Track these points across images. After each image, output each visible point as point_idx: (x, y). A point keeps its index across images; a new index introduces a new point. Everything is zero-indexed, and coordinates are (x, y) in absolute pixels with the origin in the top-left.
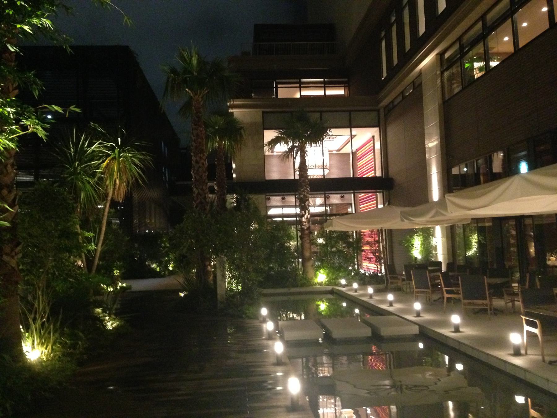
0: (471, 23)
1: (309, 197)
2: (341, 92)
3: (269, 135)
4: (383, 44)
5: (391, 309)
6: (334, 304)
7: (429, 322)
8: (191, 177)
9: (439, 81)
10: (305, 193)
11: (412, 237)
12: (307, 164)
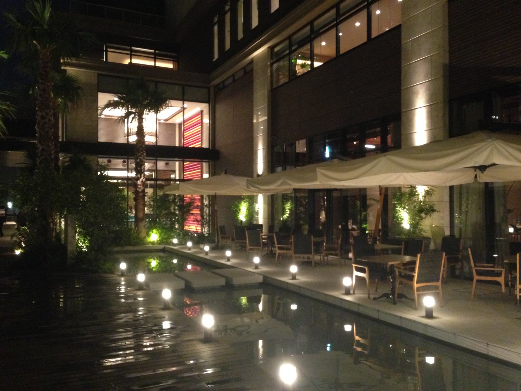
0: (300, 26)
1: (145, 162)
2: (169, 65)
3: (103, 98)
4: (216, 28)
5: (228, 263)
6: (165, 261)
7: (269, 273)
8: (35, 132)
9: (269, 71)
10: (142, 158)
11: (240, 203)
12: (144, 131)
